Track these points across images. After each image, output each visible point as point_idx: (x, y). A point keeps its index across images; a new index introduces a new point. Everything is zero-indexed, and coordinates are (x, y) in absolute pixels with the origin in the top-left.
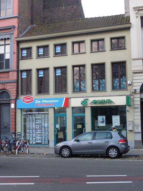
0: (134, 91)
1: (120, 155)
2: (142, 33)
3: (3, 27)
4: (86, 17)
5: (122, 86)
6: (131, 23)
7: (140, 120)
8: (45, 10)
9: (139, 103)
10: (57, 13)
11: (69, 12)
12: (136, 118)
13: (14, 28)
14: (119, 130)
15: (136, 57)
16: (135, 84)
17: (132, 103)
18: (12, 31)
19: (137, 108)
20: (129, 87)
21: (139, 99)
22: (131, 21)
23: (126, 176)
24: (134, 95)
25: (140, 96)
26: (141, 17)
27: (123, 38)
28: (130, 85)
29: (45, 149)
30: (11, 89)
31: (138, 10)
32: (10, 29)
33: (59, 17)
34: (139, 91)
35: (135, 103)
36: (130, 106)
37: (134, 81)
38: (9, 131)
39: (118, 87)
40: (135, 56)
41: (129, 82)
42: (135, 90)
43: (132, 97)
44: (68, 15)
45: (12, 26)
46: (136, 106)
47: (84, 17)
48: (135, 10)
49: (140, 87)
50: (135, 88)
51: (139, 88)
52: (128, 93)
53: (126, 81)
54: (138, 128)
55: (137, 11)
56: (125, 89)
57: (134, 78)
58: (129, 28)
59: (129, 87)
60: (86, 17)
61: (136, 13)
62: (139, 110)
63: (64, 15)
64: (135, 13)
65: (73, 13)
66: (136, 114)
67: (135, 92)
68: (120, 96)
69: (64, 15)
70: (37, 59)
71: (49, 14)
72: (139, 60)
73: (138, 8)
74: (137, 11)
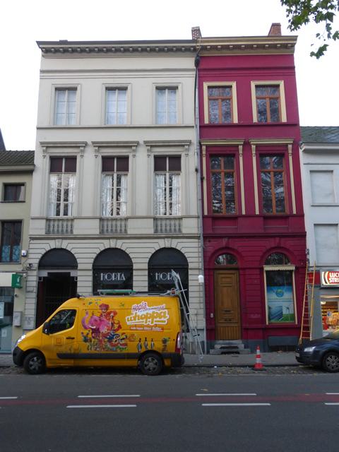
0: (28, 266)
1: (163, 371)
4: (8, 148)
5: (14, 257)
6: (34, 165)
9: (35, 284)
12: (27, 306)
13: (189, 145)
15: (37, 215)
16: (30, 256)
17: (23, 284)
18: (134, 151)
19: (32, 292)
20: (23, 260)
21: (35, 279)
22: (35, 162)
23: (326, 404)
24: (29, 272)
25: (38, 273)
26: (50, 157)
27: (23, 184)
28: (24, 256)
29: (201, 377)
31: (151, 146)
34: (36, 266)
35: (29, 284)
36: (20, 288)
37: (31, 251)
38: (265, 351)
39: (8, 259)
40: (35, 213)
41: (23, 252)
42: (30, 264)
43: (24, 274)
46: (29, 289)
49: (148, 259)
50: (30, 261)
51: (37, 261)
52: (18, 268)
53: (20, 251)
54: (29, 323)
55: (45, 148)
56: (17, 262)
57: (31, 246)
58: (30, 172)
59: (23, 260)
60: (8, 148)
61: (44, 151)
62: (34, 295)
64: (42, 151)
66: (28, 301)
67: (30, 267)
68: (6, 272)
70: (313, 208)
72: (149, 220)
74: (45, 148)
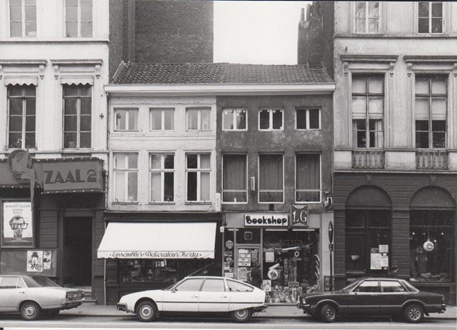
2: (369, 279)
3: (390, 41)
4: (216, 60)
7: (214, 253)
8: (139, 35)
10: (165, 45)
11: (190, 46)
14: (319, 7)
18: (98, 70)
30: (362, 13)
32: (94, 65)
33: (168, 53)
44: (187, 53)
45: (97, 60)
47: (212, 58)
48: (343, 62)
60: (216, 60)
63: (179, 51)
65: (196, 49)
69: (179, 51)
71: (148, 46)
73: (415, 59)
